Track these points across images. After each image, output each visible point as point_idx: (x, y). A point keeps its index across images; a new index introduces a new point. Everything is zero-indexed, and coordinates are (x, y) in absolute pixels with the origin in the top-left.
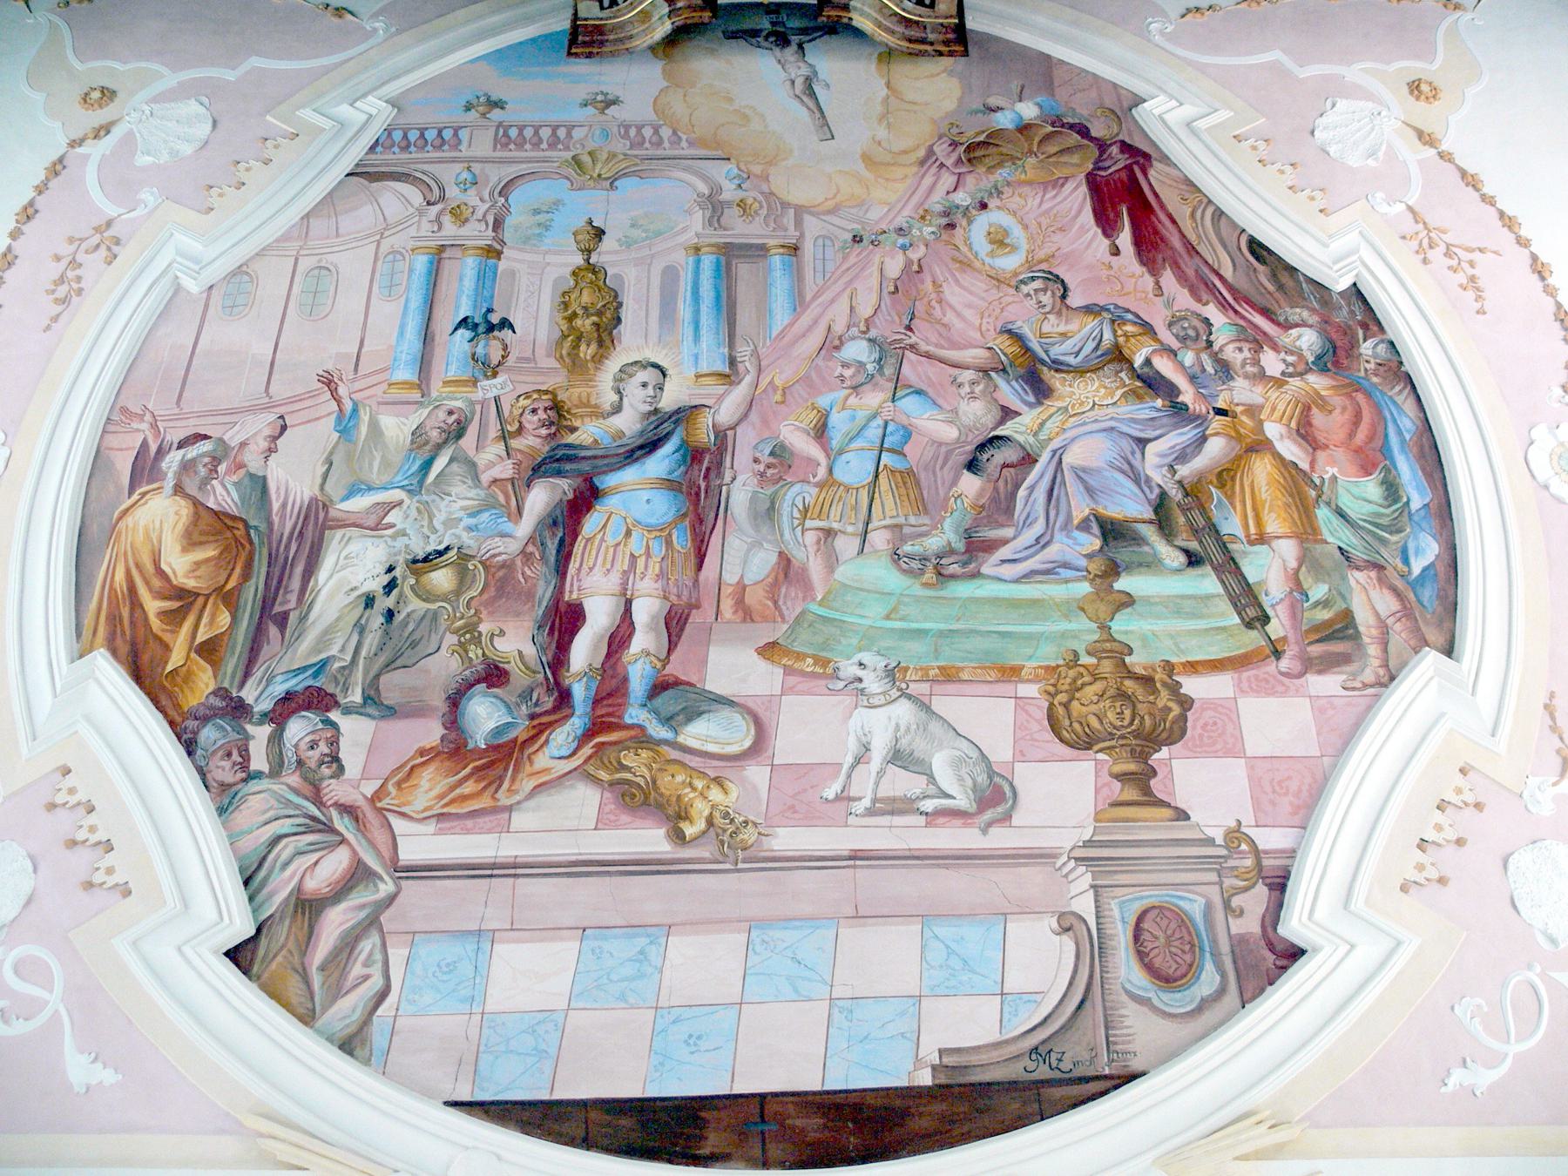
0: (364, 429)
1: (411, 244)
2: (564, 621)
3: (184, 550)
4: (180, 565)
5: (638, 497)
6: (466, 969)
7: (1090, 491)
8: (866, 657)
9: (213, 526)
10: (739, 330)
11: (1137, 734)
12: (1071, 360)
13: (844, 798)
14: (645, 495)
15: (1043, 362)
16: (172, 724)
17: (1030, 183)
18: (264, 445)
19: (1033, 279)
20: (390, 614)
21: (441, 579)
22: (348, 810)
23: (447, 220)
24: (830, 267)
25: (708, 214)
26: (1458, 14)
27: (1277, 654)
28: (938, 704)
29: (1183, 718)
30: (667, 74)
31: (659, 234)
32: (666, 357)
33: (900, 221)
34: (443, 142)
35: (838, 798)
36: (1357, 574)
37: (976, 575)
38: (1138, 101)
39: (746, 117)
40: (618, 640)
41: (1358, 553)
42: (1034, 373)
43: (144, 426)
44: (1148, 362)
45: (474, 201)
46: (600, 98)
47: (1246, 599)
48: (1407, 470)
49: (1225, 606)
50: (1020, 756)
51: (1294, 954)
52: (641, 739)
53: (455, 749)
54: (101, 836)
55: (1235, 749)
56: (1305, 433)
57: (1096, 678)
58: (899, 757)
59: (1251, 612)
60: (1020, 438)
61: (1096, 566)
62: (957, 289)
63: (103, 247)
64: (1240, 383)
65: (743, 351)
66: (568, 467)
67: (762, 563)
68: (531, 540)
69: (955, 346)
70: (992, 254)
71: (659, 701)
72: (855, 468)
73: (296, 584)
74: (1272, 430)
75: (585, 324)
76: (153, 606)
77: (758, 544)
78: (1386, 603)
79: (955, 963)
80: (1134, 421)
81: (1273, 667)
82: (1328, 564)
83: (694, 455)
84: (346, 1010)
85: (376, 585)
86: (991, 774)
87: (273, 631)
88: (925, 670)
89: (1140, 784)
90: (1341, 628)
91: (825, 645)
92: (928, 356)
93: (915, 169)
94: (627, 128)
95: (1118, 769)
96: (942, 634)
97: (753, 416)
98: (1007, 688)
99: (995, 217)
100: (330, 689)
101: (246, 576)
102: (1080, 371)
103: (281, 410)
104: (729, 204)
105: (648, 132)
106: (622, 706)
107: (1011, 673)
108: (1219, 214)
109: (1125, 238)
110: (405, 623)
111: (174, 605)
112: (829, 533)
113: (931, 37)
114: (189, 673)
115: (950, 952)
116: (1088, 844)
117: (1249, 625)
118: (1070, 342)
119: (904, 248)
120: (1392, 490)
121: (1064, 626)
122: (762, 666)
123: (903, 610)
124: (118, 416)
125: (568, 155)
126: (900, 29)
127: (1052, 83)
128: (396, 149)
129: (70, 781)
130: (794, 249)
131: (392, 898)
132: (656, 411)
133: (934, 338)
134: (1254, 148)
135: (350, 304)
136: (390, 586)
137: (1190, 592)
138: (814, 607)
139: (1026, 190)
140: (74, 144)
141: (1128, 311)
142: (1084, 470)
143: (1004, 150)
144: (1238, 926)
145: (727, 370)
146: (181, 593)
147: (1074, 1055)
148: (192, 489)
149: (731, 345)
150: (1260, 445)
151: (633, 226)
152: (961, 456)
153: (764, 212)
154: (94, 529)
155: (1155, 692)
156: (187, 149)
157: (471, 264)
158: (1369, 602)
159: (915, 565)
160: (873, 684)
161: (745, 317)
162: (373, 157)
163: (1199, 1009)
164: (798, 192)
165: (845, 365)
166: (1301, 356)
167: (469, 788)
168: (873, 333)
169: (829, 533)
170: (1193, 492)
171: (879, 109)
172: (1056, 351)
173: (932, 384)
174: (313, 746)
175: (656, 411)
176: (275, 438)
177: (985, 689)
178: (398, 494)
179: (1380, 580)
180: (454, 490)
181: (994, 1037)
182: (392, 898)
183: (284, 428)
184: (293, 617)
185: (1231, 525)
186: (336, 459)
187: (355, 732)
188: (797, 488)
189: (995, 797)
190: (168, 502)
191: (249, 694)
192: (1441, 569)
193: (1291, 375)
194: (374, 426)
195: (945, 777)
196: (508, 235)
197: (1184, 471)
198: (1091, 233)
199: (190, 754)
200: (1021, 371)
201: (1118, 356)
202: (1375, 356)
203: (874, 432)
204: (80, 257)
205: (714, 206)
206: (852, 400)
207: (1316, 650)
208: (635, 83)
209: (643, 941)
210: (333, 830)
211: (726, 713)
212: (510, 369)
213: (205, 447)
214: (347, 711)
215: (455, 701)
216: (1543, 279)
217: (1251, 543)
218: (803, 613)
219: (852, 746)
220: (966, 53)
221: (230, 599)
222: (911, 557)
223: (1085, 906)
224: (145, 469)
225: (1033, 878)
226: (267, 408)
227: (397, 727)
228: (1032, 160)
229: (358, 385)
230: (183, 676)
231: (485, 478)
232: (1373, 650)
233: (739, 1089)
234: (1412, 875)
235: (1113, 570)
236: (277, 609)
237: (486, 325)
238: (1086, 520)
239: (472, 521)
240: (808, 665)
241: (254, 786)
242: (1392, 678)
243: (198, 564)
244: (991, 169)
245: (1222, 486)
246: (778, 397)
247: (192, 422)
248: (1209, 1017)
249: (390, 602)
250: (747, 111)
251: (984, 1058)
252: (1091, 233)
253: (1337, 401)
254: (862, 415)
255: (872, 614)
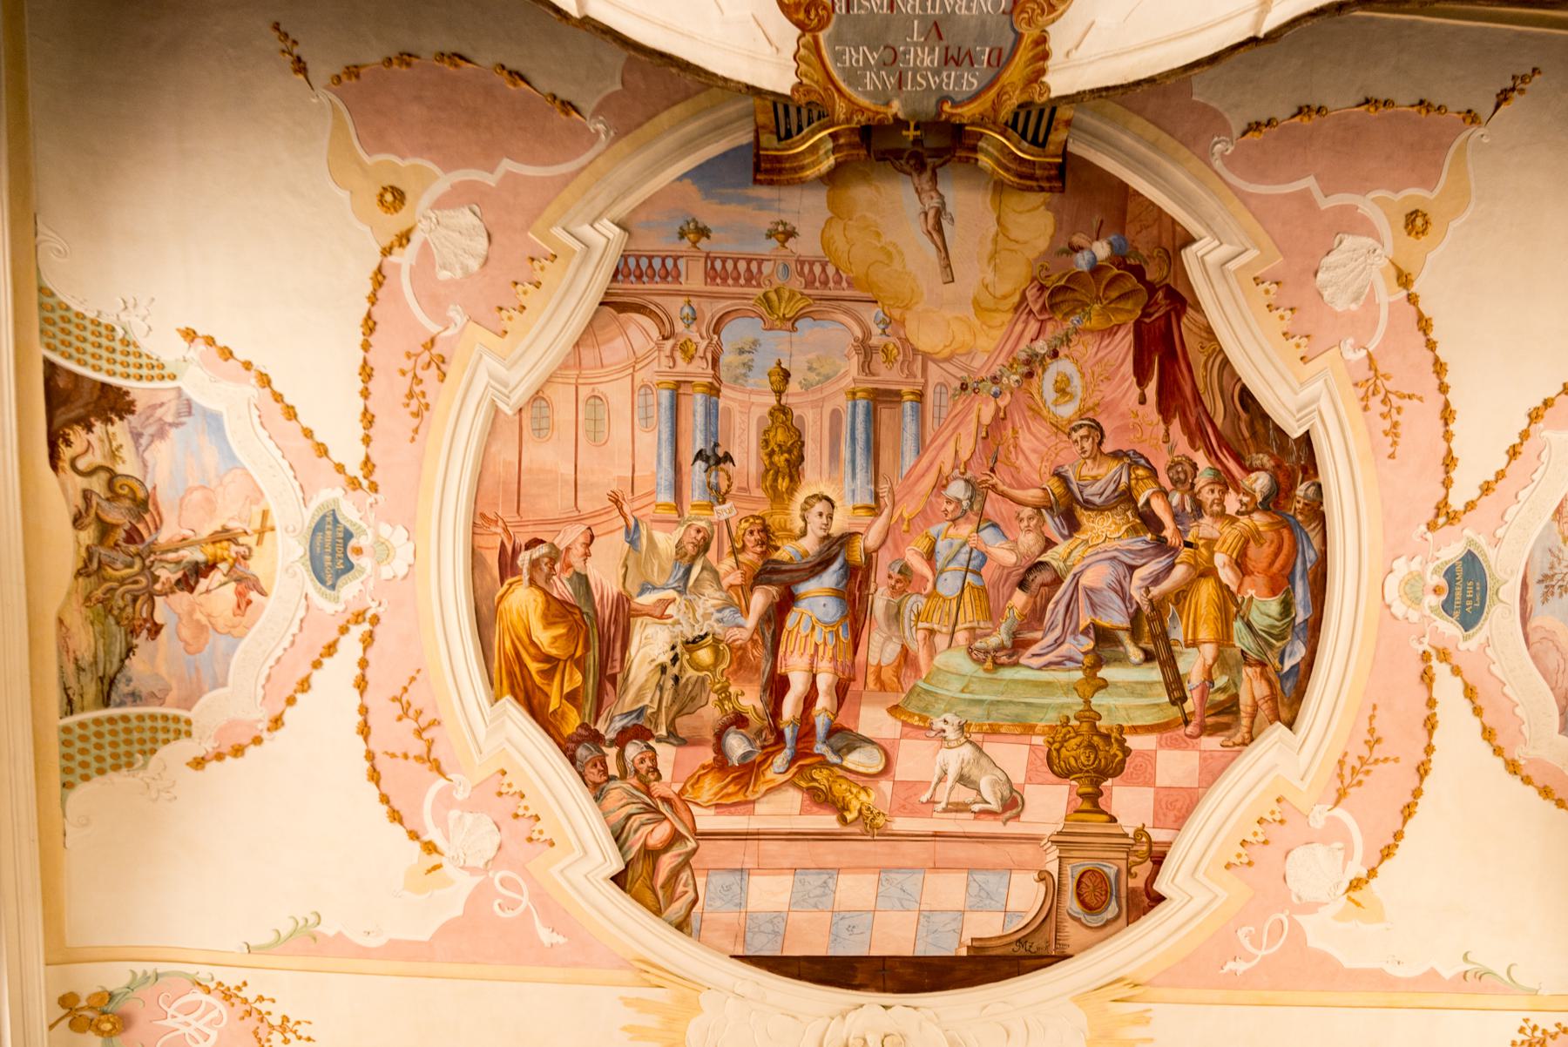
0: (644, 541)
1: (657, 379)
2: (777, 686)
3: (545, 628)
4: (544, 637)
5: (818, 600)
6: (736, 889)
7: (1093, 605)
8: (948, 716)
9: (557, 611)
10: (881, 471)
11: (1096, 770)
12: (1097, 500)
13: (931, 802)
14: (822, 601)
15: (1078, 502)
16: (559, 745)
17: (1092, 331)
18: (581, 550)
19: (1081, 426)
20: (676, 679)
21: (705, 655)
22: (665, 800)
23: (678, 355)
24: (944, 414)
25: (862, 358)
26: (1474, 127)
27: (1187, 723)
28: (987, 748)
29: (1123, 761)
30: (832, 205)
31: (828, 378)
32: (832, 493)
33: (995, 370)
34: (668, 273)
35: (928, 802)
36: (1249, 670)
37: (1016, 664)
38: (1190, 240)
39: (889, 255)
40: (809, 700)
41: (1253, 655)
42: (1068, 510)
43: (499, 530)
44: (1148, 502)
45: (696, 338)
46: (781, 228)
47: (1175, 686)
48: (1301, 591)
49: (1162, 690)
50: (1029, 780)
51: (1159, 899)
52: (825, 764)
53: (721, 763)
54: (531, 812)
55: (1150, 782)
56: (1241, 564)
57: (1077, 734)
58: (963, 779)
59: (1177, 694)
60: (1055, 564)
61: (1088, 661)
62: (1028, 436)
63: (434, 366)
64: (1207, 520)
65: (884, 488)
66: (775, 577)
67: (891, 652)
68: (756, 630)
69: (1022, 486)
70: (1056, 403)
71: (832, 740)
72: (949, 585)
73: (618, 655)
74: (1220, 559)
75: (781, 460)
76: (533, 667)
77: (889, 638)
78: (1261, 689)
79: (983, 894)
80: (1130, 551)
81: (1181, 732)
82: (1231, 662)
83: (850, 571)
84: (677, 909)
85: (666, 658)
86: (1012, 790)
87: (609, 687)
88: (981, 726)
89: (1093, 800)
90: (1230, 707)
91: (926, 709)
92: (1003, 494)
93: (1009, 316)
94: (802, 263)
95: (1082, 790)
96: (992, 703)
97: (889, 543)
98: (1026, 739)
99: (1063, 366)
100: (648, 726)
101: (587, 647)
102: (1100, 509)
103: (589, 522)
104: (876, 348)
105: (817, 269)
106: (812, 742)
107: (1029, 729)
108: (1226, 362)
109: (1152, 388)
110: (686, 685)
111: (546, 666)
112: (932, 632)
113: (1038, 172)
114: (563, 713)
115: (981, 888)
116: (1060, 833)
117: (1173, 703)
118: (1098, 484)
119: (996, 396)
120: (1287, 607)
121: (1064, 700)
122: (890, 720)
123: (972, 687)
124: (479, 522)
125: (759, 292)
126: (1013, 166)
127: (1124, 213)
128: (632, 278)
129: (507, 779)
130: (920, 396)
131: (695, 851)
132: (828, 537)
133: (1008, 479)
134: (1267, 292)
135: (620, 431)
136: (675, 659)
137: (1142, 679)
138: (920, 683)
139: (1089, 336)
140: (387, 252)
141: (1142, 456)
142: (1092, 589)
143: (1078, 296)
144: (1132, 883)
145: (873, 504)
146: (548, 658)
147: (1037, 943)
148: (541, 583)
149: (876, 483)
150: (1209, 572)
151: (810, 369)
152: (1014, 579)
153: (900, 358)
154: (484, 610)
155: (1110, 744)
156: (474, 265)
157: (699, 399)
158: (1252, 688)
159: (981, 656)
160: (951, 734)
161: (886, 456)
162: (615, 285)
163: (1104, 926)
164: (927, 338)
165: (949, 502)
166: (1253, 497)
167: (731, 789)
168: (969, 475)
169: (932, 632)
170: (1157, 606)
171: (989, 247)
172: (1088, 491)
173: (1003, 519)
174: (642, 761)
175: (828, 537)
176: (588, 545)
177: (1013, 738)
178: (671, 594)
179: (1262, 674)
180: (706, 592)
181: (999, 933)
182: (695, 851)
183: (592, 537)
184: (619, 677)
185: (1178, 633)
186: (630, 563)
187: (666, 754)
188: (914, 598)
189: (1012, 804)
190: (528, 591)
191: (601, 727)
192: (1302, 667)
193: (1242, 514)
194: (651, 539)
195: (987, 792)
196: (723, 374)
197: (1155, 591)
198: (1127, 384)
199: (573, 764)
200: (1062, 508)
201: (1126, 497)
202: (1305, 497)
203: (963, 557)
204: (420, 373)
205: (866, 350)
206: (952, 531)
207: (1210, 721)
208: (806, 209)
209: (825, 877)
210: (660, 812)
211: (869, 748)
212: (734, 497)
213: (542, 550)
214: (659, 740)
215: (720, 736)
216: (1446, 424)
217: (1187, 646)
218: (915, 686)
219: (938, 771)
220: (1062, 190)
221: (580, 663)
222: (978, 650)
223: (1053, 868)
224: (508, 566)
225: (1028, 850)
226: (580, 520)
227: (689, 751)
228: (1097, 306)
229: (637, 505)
230: (559, 715)
231: (725, 583)
232: (1245, 722)
233: (874, 953)
234: (1233, 860)
235: (1099, 663)
236: (609, 672)
237: (715, 458)
238: (1087, 628)
239: (719, 615)
240: (916, 721)
241: (613, 784)
242: (1252, 740)
243: (556, 638)
244: (1066, 315)
245: (1177, 603)
246: (905, 527)
247: (530, 529)
248: (1109, 929)
249: (675, 670)
250: (890, 248)
251: (993, 943)
252: (1127, 384)
253: (1270, 535)
254: (957, 543)
255: (953, 689)
